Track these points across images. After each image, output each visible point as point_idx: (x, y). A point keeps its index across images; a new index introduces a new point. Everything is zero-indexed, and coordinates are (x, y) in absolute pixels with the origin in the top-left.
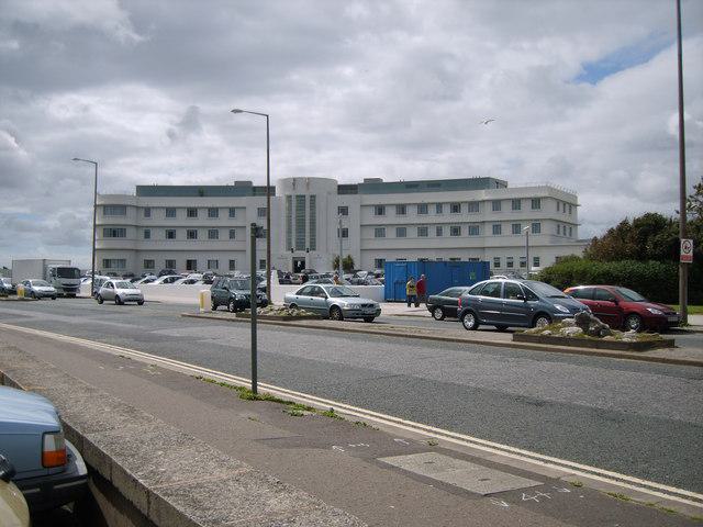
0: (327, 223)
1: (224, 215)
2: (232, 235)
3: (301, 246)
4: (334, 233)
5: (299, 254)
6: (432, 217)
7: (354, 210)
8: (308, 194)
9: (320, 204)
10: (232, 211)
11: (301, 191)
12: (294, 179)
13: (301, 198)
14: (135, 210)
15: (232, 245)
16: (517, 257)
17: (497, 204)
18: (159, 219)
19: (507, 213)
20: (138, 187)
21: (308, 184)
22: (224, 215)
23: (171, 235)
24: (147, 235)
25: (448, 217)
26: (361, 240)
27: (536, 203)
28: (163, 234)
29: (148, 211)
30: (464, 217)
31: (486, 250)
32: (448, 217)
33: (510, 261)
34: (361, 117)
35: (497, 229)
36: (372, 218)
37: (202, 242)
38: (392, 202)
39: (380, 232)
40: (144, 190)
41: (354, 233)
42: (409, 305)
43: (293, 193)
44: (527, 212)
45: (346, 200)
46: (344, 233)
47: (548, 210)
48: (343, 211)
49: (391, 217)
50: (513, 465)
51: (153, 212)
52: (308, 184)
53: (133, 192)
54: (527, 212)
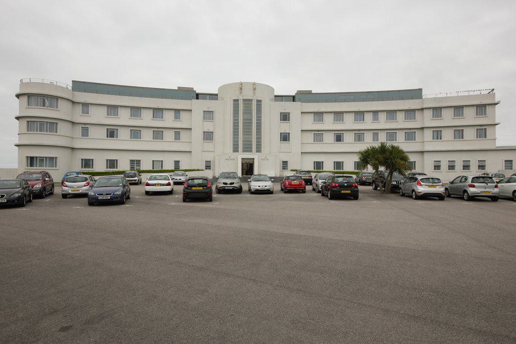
0: (271, 127)
2: (339, 138)
3: (248, 148)
7: (295, 116)
8: (255, 98)
10: (177, 111)
11: (248, 94)
12: (241, 84)
13: (248, 102)
15: (339, 147)
17: (410, 113)
19: (427, 120)
20: (73, 81)
23: (111, 134)
27: (458, 109)
28: (103, 132)
29: (86, 105)
31: (426, 155)
35: (459, 133)
36: (310, 123)
39: (318, 135)
40: (79, 86)
41: (295, 136)
42: (135, 163)
45: (288, 107)
46: (285, 137)
48: (285, 117)
49: (329, 123)
50: (86, 172)
54: (448, 118)
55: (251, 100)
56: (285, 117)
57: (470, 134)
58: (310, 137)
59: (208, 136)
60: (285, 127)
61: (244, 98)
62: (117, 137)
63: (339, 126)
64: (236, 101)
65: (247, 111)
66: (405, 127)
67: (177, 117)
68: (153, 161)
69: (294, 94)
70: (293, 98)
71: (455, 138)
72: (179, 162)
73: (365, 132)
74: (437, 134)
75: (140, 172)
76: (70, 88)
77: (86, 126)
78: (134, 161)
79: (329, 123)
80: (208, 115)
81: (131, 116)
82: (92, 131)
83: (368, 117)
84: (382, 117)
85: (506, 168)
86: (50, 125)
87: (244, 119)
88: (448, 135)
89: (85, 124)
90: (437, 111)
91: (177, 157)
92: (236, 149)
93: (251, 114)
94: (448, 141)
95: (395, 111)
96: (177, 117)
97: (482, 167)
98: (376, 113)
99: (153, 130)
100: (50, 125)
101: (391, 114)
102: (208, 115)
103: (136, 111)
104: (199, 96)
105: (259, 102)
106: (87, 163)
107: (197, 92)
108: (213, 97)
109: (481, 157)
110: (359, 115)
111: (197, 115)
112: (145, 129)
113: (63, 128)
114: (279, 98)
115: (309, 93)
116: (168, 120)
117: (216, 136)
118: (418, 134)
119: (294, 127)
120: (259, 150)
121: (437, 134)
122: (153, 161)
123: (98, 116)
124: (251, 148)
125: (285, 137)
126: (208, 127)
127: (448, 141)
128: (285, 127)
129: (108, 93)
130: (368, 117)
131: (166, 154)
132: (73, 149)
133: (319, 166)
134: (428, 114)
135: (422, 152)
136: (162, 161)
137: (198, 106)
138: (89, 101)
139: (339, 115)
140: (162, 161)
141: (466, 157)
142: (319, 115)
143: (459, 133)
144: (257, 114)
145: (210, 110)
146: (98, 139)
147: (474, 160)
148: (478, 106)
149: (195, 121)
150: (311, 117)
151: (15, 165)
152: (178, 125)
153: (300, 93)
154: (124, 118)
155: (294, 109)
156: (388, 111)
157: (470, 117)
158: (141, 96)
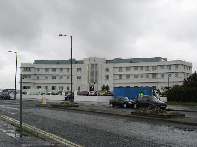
0: (102, 74)
3: (92, 82)
6: (139, 71)
7: (111, 69)
11: (92, 62)
13: (92, 65)
19: (166, 70)
21: (90, 60)
24: (38, 77)
29: (39, 69)
30: (151, 71)
32: (144, 71)
35: (61, 77)
36: (117, 72)
39: (120, 77)
45: (108, 65)
46: (107, 77)
48: (107, 69)
52: (90, 60)
53: (34, 62)
55: (93, 64)
56: (107, 69)
58: (117, 77)
60: (107, 74)
63: (46, 73)
65: (92, 68)
66: (134, 73)
73: (31, 75)
75: (15, 90)
76: (34, 64)
77: (30, 75)
80: (79, 70)
82: (40, 77)
84: (144, 68)
86: (28, 76)
89: (38, 75)
90: (169, 66)
95: (149, 66)
98: (141, 67)
100: (28, 76)
101: (147, 67)
102: (79, 70)
108: (81, 62)
110: (136, 68)
112: (165, 73)
113: (32, 77)
114: (107, 62)
117: (82, 77)
119: (110, 74)
125: (107, 77)
126: (79, 74)
129: (46, 64)
130: (139, 69)
131: (64, 84)
132: (35, 83)
135: (158, 82)
138: (121, 66)
139: (47, 69)
142: (120, 68)
150: (118, 69)
154: (124, 72)
156: (146, 66)
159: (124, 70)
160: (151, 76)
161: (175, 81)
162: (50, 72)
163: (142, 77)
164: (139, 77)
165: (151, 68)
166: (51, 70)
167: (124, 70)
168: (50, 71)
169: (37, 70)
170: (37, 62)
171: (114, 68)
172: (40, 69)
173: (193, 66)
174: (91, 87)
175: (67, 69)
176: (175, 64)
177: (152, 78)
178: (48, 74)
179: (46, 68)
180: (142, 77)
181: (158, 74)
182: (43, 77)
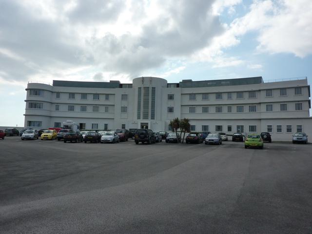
0: (162, 104)
1: (102, 98)
3: (146, 117)
4: (165, 110)
5: (145, 121)
6: (225, 100)
7: (177, 97)
8: (151, 87)
9: (157, 93)
11: (147, 84)
13: (147, 89)
14: (50, 93)
16: (284, 125)
17: (252, 93)
18: (64, 99)
19: (262, 98)
21: (151, 81)
22: (102, 98)
24: (57, 109)
25: (235, 100)
26: (181, 114)
29: (58, 94)
30: (246, 100)
31: (262, 121)
32: (235, 100)
33: (270, 127)
34: (229, 51)
35: (284, 107)
36: (187, 101)
37: (89, 113)
38: (225, 91)
43: (142, 86)
44: (276, 97)
47: (291, 96)
48: (171, 97)
49: (199, 101)
51: (61, 95)
52: (151, 81)
53: (51, 84)
54: (276, 97)
56: (171, 97)
57: (291, 107)
58: (187, 110)
59: (124, 110)
60: (171, 104)
61: (145, 86)
62: (302, 109)
63: (72, 101)
64: (140, 88)
65: (147, 94)
67: (107, 98)
68: (93, 124)
69: (179, 82)
70: (178, 85)
71: (267, 110)
72: (107, 125)
74: (269, 107)
77: (285, 103)
78: (239, 126)
79: (199, 101)
80: (124, 97)
81: (281, 95)
82: (61, 107)
83: (225, 96)
84: (234, 96)
85: (123, 128)
87: (144, 99)
88: (277, 108)
89: (57, 103)
90: (269, 91)
91: (106, 122)
92: (139, 118)
93: (149, 95)
94: (277, 113)
96: (107, 98)
97: (299, 130)
99: (249, 105)
101: (240, 94)
102: (124, 97)
103: (205, 96)
104: (123, 86)
105: (154, 89)
106: (57, 124)
107: (121, 83)
109: (299, 123)
110: (240, 94)
111: (118, 97)
113: (46, 106)
115: (190, 81)
116: (102, 101)
118: (258, 107)
120: (153, 117)
121: (269, 107)
122: (93, 124)
123: (64, 99)
124: (148, 117)
126: (124, 104)
127: (277, 113)
128: (171, 104)
130: (225, 96)
133: (81, 127)
134: (263, 94)
135: (260, 119)
136: (97, 124)
137: (118, 92)
139: (84, 96)
140: (97, 124)
141: (289, 123)
143: (284, 107)
144: (152, 96)
145: (126, 94)
146: (64, 112)
147: (294, 125)
148: (296, 88)
149: (117, 101)
150: (188, 96)
151: (23, 126)
152: (107, 103)
153: (185, 82)
155: (177, 92)
157: (291, 96)
158: (240, 84)
159: (199, 98)
160: (246, 108)
161: (299, 117)
162: (78, 100)
163: (230, 110)
164: (225, 109)
165: (246, 95)
166: (92, 96)
167: (199, 98)
168: (78, 97)
169: (55, 95)
170: (56, 83)
171: (182, 94)
172: (61, 95)
173: (25, 102)
174: (143, 125)
175: (105, 95)
176: (296, 86)
177: (227, 112)
178: (221, 103)
179: (70, 93)
180: (230, 110)
181: (262, 105)
182: (66, 108)
